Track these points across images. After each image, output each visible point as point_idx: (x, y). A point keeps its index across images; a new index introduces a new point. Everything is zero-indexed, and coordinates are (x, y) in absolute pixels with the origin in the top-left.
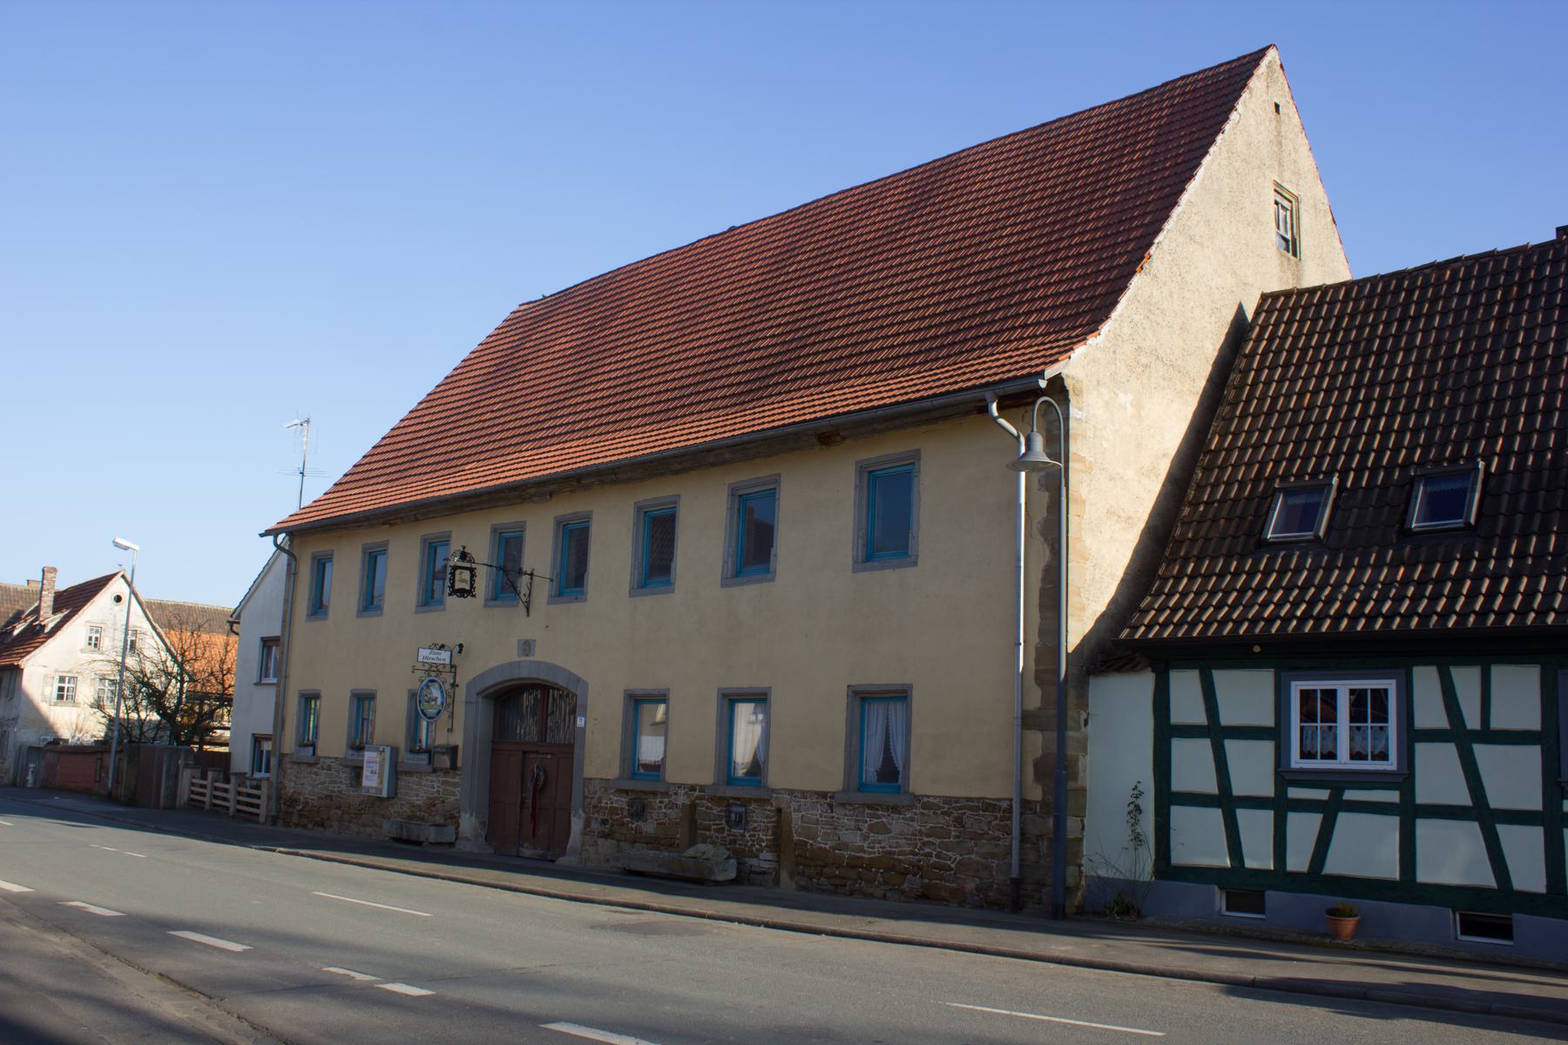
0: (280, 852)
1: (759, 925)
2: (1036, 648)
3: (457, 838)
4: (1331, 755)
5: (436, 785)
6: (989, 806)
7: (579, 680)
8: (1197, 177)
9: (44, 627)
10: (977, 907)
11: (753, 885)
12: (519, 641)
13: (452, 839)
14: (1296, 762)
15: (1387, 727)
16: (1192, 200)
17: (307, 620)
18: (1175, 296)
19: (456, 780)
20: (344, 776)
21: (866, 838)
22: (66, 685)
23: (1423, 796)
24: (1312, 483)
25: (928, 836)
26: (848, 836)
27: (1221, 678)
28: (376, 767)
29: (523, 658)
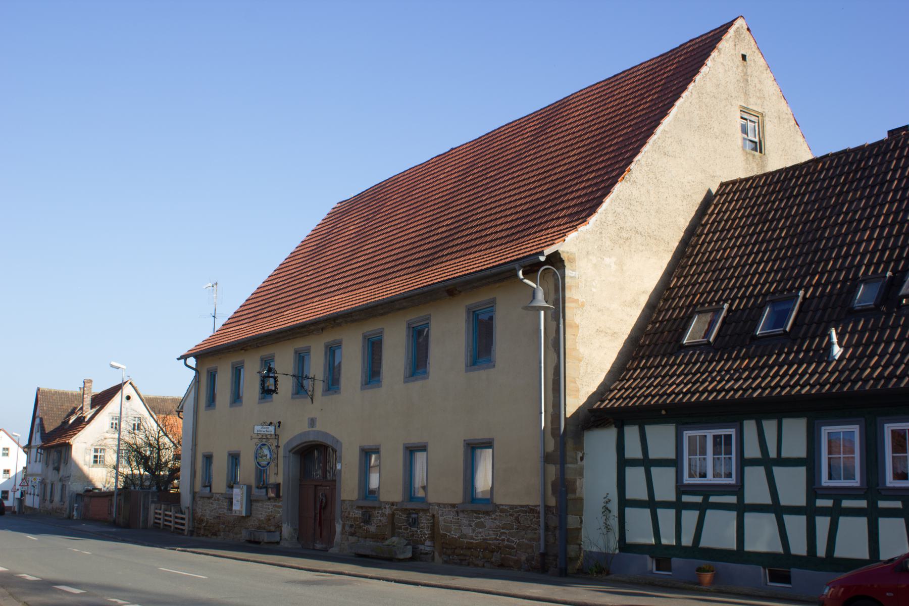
0: (178, 550)
1: (391, 581)
3: (281, 539)
5: (270, 507)
6: (531, 510)
7: (338, 441)
8: (671, 115)
9: (85, 417)
11: (421, 561)
12: (309, 418)
13: (278, 539)
14: (687, 480)
16: (666, 130)
17: (206, 410)
18: (652, 192)
19: (280, 504)
21: (474, 531)
22: (99, 454)
23: (748, 500)
24: (716, 307)
25: (503, 529)
26: (468, 531)
29: (311, 429)
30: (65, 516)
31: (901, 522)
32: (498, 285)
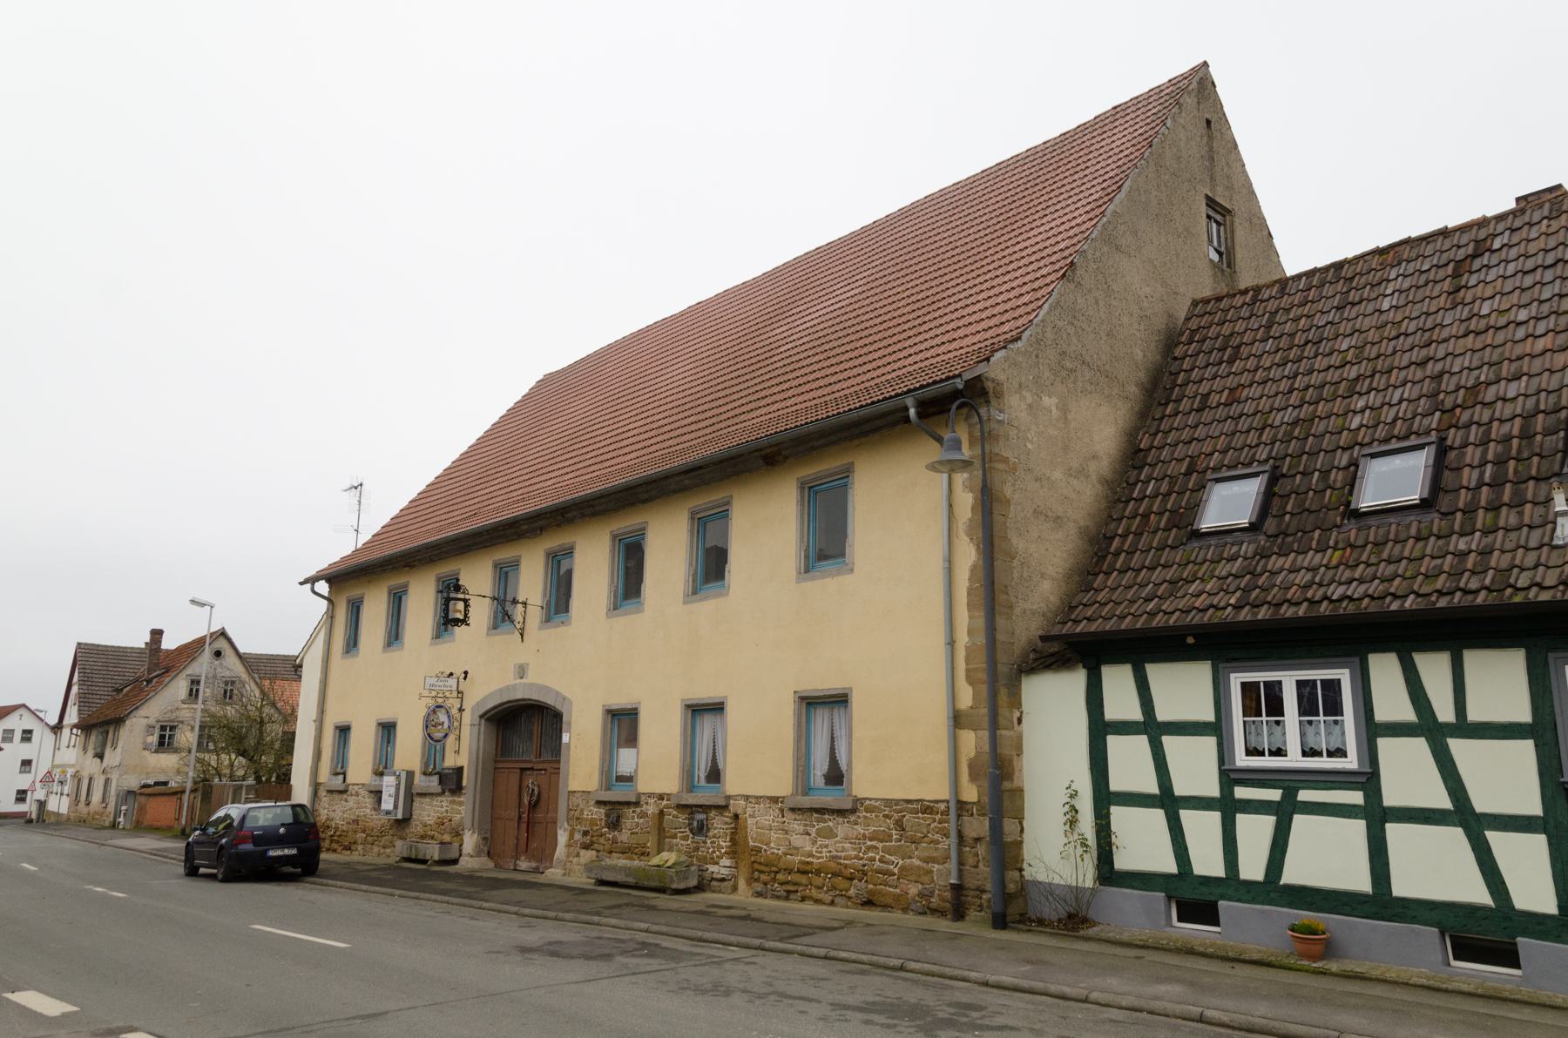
2: (966, 647)
4: (1279, 752)
6: (927, 808)
10: (920, 913)
14: (1242, 760)
15: (1343, 721)
18: (1101, 303)
20: (369, 801)
21: (814, 843)
23: (1390, 799)
25: (871, 840)
26: (797, 840)
27: (1155, 672)
28: (393, 790)
29: (519, 681)
30: (107, 824)
31: (1540, 841)
32: (856, 442)
